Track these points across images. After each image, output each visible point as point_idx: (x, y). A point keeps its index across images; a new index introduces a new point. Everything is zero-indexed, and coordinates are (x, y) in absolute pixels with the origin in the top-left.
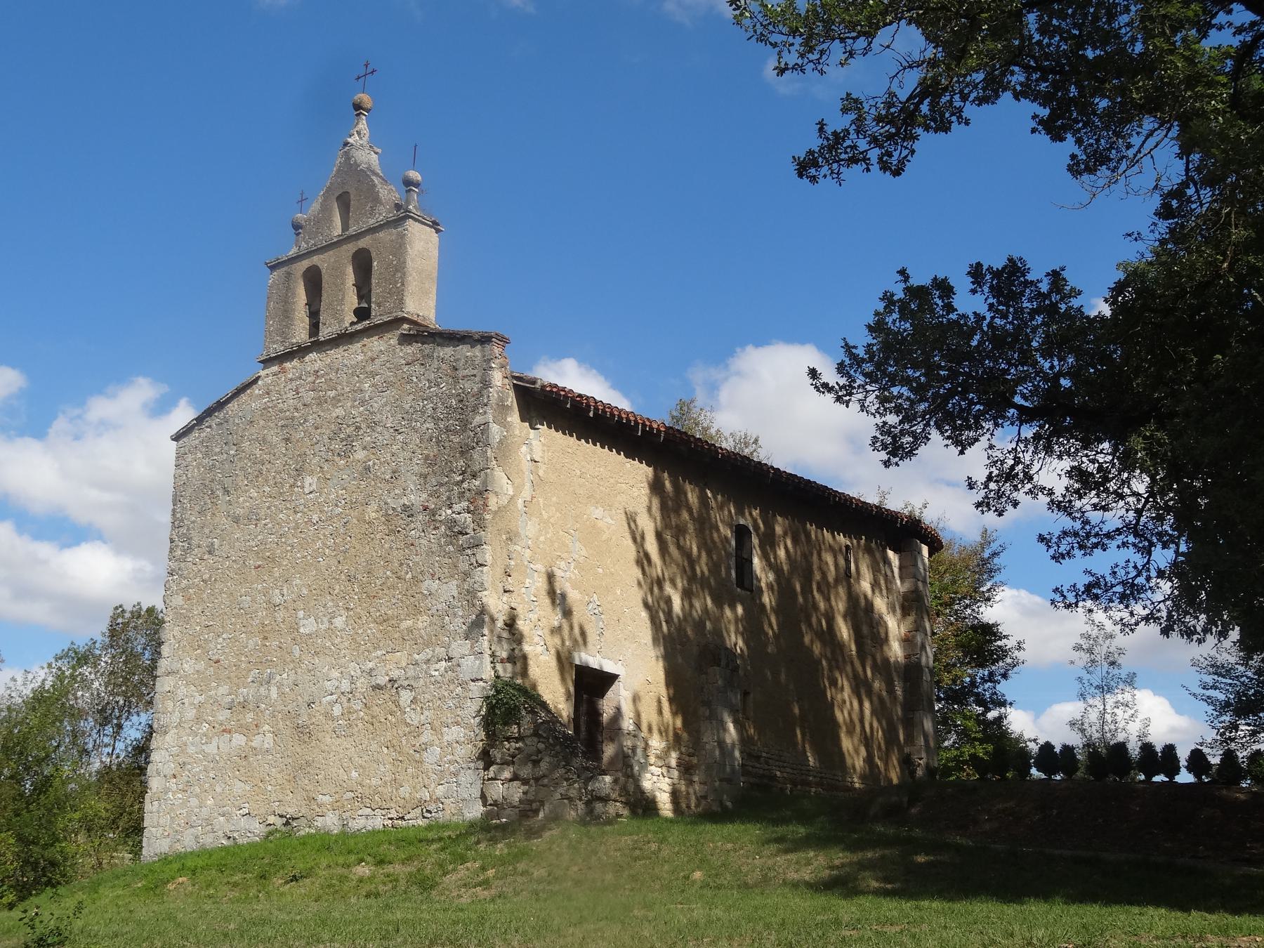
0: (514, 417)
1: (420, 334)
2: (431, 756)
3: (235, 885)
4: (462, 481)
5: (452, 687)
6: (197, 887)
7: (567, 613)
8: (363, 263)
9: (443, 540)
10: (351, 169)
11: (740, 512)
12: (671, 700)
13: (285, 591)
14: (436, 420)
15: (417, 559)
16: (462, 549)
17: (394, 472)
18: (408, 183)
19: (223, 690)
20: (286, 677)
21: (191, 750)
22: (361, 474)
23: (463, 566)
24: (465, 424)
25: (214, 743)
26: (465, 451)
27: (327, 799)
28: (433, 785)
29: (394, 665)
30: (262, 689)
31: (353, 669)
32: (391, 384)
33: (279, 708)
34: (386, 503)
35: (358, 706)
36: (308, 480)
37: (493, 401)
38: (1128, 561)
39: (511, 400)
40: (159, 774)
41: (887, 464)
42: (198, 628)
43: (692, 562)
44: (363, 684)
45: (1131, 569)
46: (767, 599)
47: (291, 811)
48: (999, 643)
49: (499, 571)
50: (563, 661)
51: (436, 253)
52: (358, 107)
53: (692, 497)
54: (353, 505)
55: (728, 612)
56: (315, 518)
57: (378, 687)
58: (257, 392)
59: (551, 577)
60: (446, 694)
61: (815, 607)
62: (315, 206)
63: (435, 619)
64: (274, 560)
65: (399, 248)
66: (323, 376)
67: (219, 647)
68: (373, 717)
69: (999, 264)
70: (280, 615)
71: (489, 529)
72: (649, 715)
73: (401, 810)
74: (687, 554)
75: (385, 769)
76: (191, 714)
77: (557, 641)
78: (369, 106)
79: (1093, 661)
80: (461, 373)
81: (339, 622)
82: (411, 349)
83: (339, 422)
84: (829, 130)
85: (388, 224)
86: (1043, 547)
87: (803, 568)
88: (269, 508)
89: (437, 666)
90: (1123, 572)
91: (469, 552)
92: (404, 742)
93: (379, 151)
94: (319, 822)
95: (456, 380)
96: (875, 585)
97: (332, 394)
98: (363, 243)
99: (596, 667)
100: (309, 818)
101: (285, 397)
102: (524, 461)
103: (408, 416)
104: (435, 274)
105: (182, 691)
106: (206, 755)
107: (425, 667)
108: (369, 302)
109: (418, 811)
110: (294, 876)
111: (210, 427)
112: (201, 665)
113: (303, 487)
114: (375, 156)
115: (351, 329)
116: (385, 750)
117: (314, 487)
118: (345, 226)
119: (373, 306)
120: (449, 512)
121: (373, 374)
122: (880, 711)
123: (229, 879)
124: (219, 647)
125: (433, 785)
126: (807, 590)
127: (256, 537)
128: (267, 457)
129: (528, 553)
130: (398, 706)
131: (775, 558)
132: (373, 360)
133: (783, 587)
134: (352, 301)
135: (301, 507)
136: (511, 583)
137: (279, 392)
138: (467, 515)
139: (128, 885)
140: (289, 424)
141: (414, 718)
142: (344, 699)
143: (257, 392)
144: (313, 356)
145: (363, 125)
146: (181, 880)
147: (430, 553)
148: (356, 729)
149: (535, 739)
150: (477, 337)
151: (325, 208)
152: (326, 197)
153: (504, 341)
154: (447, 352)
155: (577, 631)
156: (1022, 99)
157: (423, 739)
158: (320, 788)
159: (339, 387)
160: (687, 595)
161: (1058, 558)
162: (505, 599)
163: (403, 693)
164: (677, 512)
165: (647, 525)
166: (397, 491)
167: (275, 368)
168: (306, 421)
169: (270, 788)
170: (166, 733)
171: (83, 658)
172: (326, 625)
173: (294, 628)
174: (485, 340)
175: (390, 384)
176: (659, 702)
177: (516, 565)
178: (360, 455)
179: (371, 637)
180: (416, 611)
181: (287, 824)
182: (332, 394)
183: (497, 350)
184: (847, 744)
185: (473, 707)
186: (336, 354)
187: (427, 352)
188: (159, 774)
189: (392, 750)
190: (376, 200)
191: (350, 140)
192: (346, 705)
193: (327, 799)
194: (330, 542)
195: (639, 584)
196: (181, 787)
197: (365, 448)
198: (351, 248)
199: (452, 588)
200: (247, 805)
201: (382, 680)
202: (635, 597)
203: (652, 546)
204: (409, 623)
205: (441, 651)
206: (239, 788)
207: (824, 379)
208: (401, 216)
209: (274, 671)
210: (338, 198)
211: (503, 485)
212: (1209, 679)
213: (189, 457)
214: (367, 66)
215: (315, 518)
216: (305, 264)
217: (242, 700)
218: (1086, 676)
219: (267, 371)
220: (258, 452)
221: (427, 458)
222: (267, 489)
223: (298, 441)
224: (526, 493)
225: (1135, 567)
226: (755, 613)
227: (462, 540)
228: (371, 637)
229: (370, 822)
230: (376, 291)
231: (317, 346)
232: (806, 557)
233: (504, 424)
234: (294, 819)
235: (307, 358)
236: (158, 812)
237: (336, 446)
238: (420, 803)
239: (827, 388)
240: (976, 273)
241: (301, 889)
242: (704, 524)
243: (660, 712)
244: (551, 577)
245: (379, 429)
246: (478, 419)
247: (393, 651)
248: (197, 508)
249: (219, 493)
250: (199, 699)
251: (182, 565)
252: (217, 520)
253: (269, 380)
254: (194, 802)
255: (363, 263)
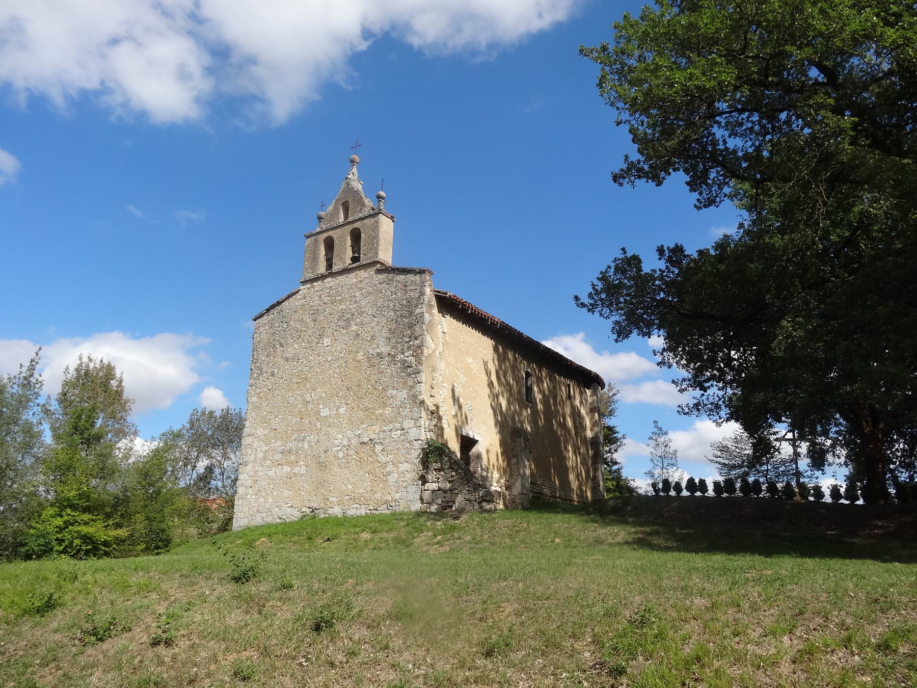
0: (435, 311)
1: (385, 269)
2: (392, 478)
3: (295, 543)
4: (410, 341)
5: (404, 443)
6: (273, 543)
7: (460, 407)
8: (356, 236)
9: (399, 370)
10: (350, 190)
11: (529, 366)
12: (502, 454)
13: (313, 395)
14: (395, 311)
15: (385, 379)
16: (409, 375)
17: (372, 336)
18: (379, 197)
19: (279, 444)
20: (313, 438)
21: (260, 474)
22: (355, 337)
23: (410, 383)
24: (411, 313)
25: (273, 470)
26: (411, 326)
27: (334, 499)
28: (393, 493)
29: (373, 432)
30: (300, 444)
31: (350, 434)
32: (372, 294)
33: (309, 453)
34: (368, 352)
35: (352, 452)
36: (326, 340)
37: (426, 302)
38: (714, 393)
39: (434, 302)
40: (242, 485)
41: (616, 341)
42: (265, 413)
43: (511, 387)
44: (354, 442)
45: (716, 397)
46: (540, 406)
47: (315, 505)
48: (615, 435)
49: (429, 386)
50: (458, 430)
51: (392, 231)
52: (352, 161)
53: (510, 356)
54: (350, 352)
55: (524, 413)
56: (329, 359)
57: (364, 443)
58: (299, 297)
59: (453, 391)
60: (401, 447)
61: (558, 411)
62: (331, 208)
63: (394, 410)
64: (307, 379)
65: (376, 227)
66: (334, 289)
67: (276, 422)
68: (360, 458)
69: (672, 246)
70: (310, 407)
71: (424, 365)
72: (493, 460)
73: (375, 505)
74: (508, 383)
75: (367, 485)
76: (261, 456)
77: (455, 421)
78: (358, 161)
79: (657, 445)
80: (409, 288)
81: (342, 410)
82: (382, 277)
83: (343, 312)
84: (630, 160)
85: (370, 216)
86: (674, 386)
87: (554, 393)
88: (304, 354)
89: (396, 433)
90: (712, 398)
91: (413, 376)
92: (377, 471)
93: (362, 183)
94: (330, 511)
95: (406, 291)
96: (581, 402)
97: (339, 298)
98: (356, 225)
99: (472, 437)
100: (325, 509)
101: (313, 299)
102: (439, 333)
103: (380, 309)
104: (392, 242)
105: (256, 444)
106: (268, 477)
107: (389, 433)
108: (359, 253)
109: (385, 506)
110: (329, 539)
111: (273, 314)
112: (267, 431)
113: (323, 344)
114: (360, 185)
115: (349, 267)
116: (367, 475)
117: (329, 343)
118: (346, 217)
119: (361, 255)
120: (402, 356)
121: (361, 289)
122: (584, 463)
123: (291, 539)
124: (276, 422)
125: (393, 493)
126: (555, 404)
127: (297, 368)
128: (304, 329)
129: (441, 378)
130: (374, 453)
131: (543, 387)
132: (361, 282)
133: (545, 401)
134: (349, 253)
135: (322, 353)
136: (434, 392)
137: (310, 297)
138: (412, 358)
139: (233, 542)
140: (315, 314)
141: (383, 459)
142: (345, 449)
143: (299, 297)
144: (329, 279)
145: (355, 170)
146: (263, 539)
147: (392, 376)
148: (351, 464)
149: (450, 470)
150: (417, 270)
151: (336, 209)
152: (336, 204)
153: (431, 273)
154: (401, 277)
155: (464, 417)
157: (388, 469)
158: (331, 494)
159: (343, 295)
160: (509, 403)
161: (682, 391)
162: (431, 400)
163: (377, 446)
164: (504, 361)
165: (492, 368)
166: (374, 346)
167: (309, 286)
168: (325, 311)
169: (303, 493)
170: (247, 465)
171: (178, 435)
172: (336, 412)
173: (318, 413)
174: (422, 272)
175: (370, 294)
176: (497, 455)
177: (436, 383)
178: (354, 328)
179: (360, 418)
180: (385, 405)
181: (313, 511)
182: (339, 298)
183: (428, 277)
184: (572, 477)
185: (415, 454)
186: (341, 279)
187: (390, 278)
188: (242, 485)
189: (371, 475)
190: (363, 205)
191: (349, 176)
192: (346, 452)
193: (334, 499)
194: (337, 371)
195: (489, 396)
196: (254, 492)
197: (357, 325)
198: (350, 228)
199: (404, 394)
200: (290, 502)
201: (366, 440)
202: (487, 402)
203: (494, 378)
204: (381, 411)
205: (398, 425)
206: (286, 493)
207: (582, 301)
208: (375, 214)
209: (306, 434)
210: (343, 204)
211: (431, 345)
212: (719, 453)
213: (262, 329)
215: (329, 359)
216: (325, 235)
217: (289, 449)
218: (654, 452)
219: (304, 287)
220: (299, 326)
221: (390, 329)
222: (303, 344)
223: (320, 321)
224: (440, 348)
225: (718, 396)
226: (535, 412)
227: (409, 370)
228: (360, 418)
229: (358, 511)
230: (363, 248)
231: (331, 273)
232: (554, 388)
233: (431, 314)
234: (316, 509)
235: (326, 281)
236: (242, 505)
237: (341, 323)
238: (386, 502)
239: (583, 305)
241: (332, 545)
242: (514, 368)
243: (498, 460)
244: (453, 391)
245: (364, 315)
246: (418, 311)
247: (372, 425)
248: (266, 354)
249: (278, 346)
250: (265, 448)
251: (257, 381)
252: (276, 359)
253: (305, 291)
254: (262, 500)
255: (356, 236)
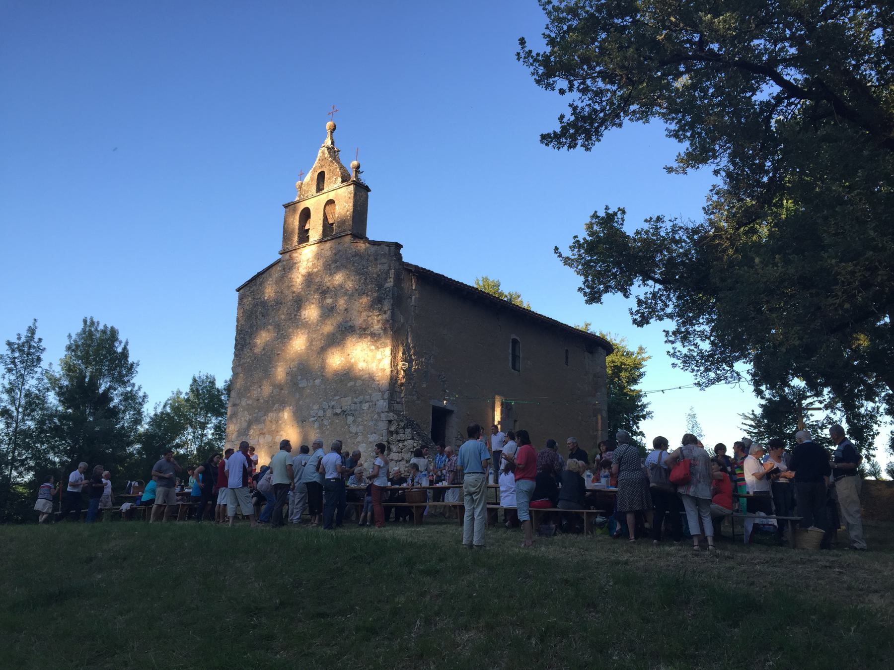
44: (329, 413)
57: (336, 414)
58: (278, 268)
141: (354, 429)
149: (413, 441)
156: (642, 370)
163: (349, 417)
201: (338, 411)
214: (334, 107)
240: (553, 90)
